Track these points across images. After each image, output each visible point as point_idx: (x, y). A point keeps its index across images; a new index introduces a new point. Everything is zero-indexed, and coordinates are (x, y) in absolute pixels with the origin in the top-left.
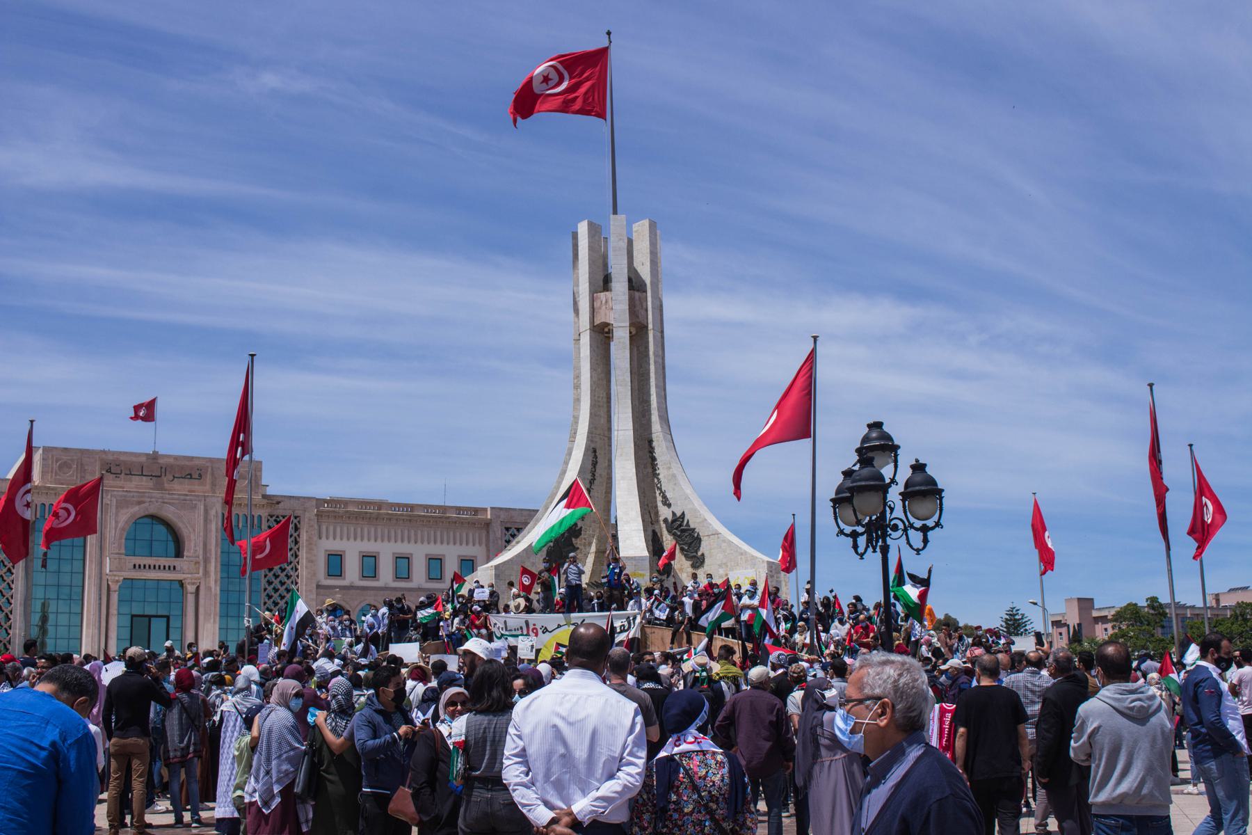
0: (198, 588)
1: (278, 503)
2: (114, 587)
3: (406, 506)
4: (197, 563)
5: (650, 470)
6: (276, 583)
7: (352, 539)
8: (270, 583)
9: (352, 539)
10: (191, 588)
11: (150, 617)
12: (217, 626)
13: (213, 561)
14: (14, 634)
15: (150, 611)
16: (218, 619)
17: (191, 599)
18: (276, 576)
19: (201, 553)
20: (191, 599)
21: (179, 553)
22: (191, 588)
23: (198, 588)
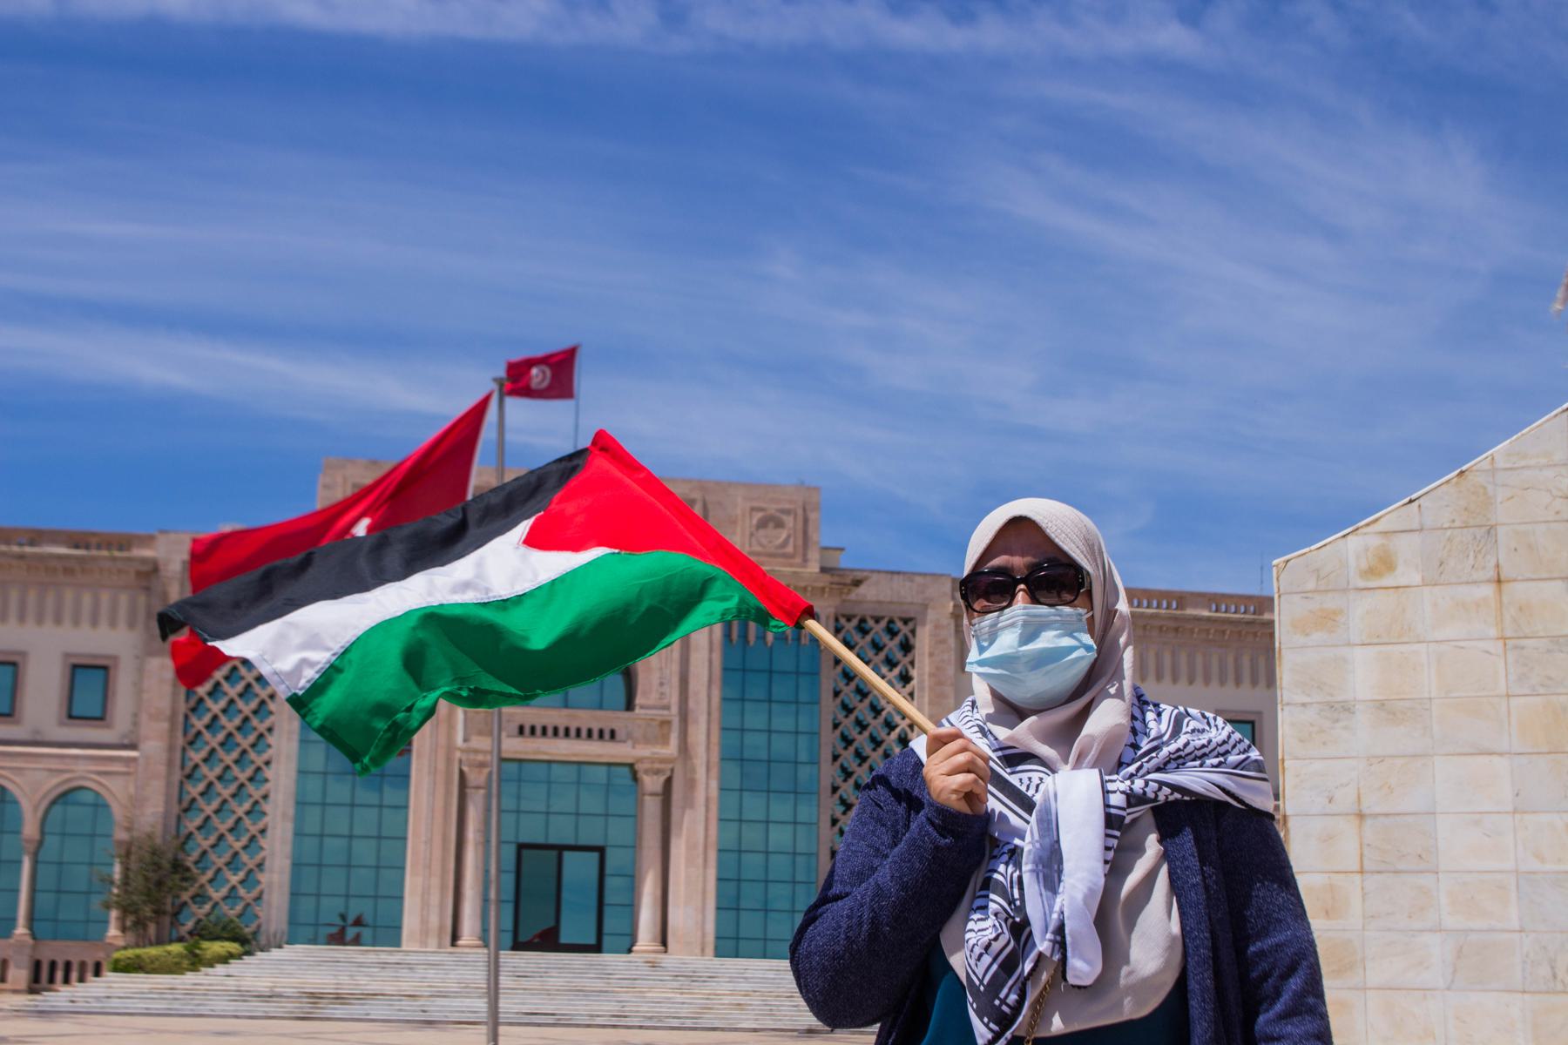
0: (668, 783)
1: (857, 583)
2: (475, 778)
3: (1167, 595)
4: (665, 723)
5: (952, 656)
6: (862, 740)
7: (1215, 683)
8: (847, 741)
9: (1215, 683)
10: (652, 783)
11: (561, 849)
12: (712, 874)
13: (703, 719)
14: (270, 885)
15: (561, 832)
16: (713, 855)
17: (493, 895)
18: (862, 726)
19: (674, 700)
20: (652, 807)
21: (629, 706)
22: (652, 783)
23: (668, 783)
